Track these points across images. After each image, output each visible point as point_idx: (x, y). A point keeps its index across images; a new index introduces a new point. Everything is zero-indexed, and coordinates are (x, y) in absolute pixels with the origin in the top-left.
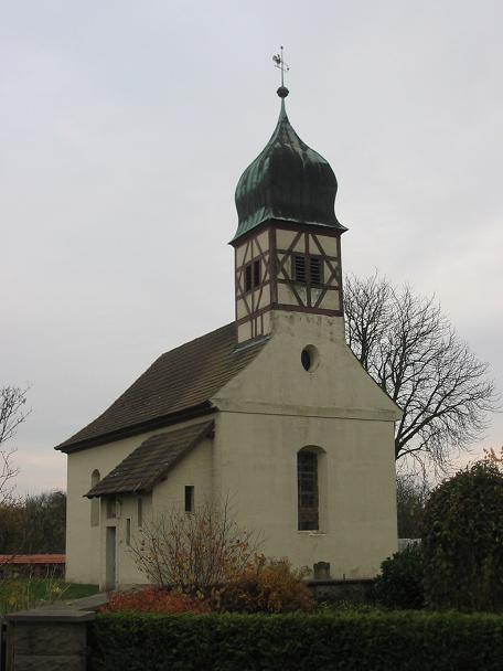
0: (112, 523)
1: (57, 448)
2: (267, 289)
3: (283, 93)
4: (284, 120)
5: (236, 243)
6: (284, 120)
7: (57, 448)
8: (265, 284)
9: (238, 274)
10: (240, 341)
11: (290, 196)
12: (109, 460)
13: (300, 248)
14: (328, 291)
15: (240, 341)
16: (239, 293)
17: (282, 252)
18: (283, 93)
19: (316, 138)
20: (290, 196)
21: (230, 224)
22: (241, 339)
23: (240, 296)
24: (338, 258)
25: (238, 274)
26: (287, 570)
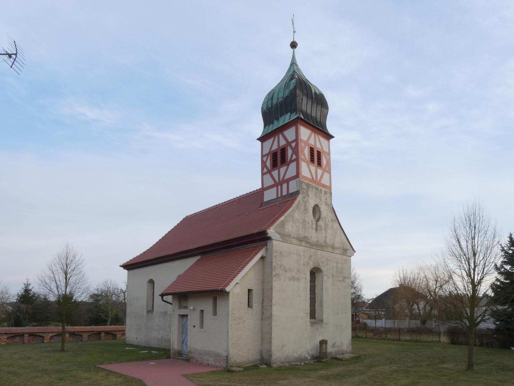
0: (183, 312)
1: (121, 266)
2: (293, 165)
3: (294, 45)
4: (293, 63)
5: (262, 139)
6: (293, 63)
7: (121, 266)
8: (292, 161)
9: (265, 159)
10: (265, 200)
11: (294, 109)
12: (167, 275)
13: (312, 142)
14: (290, 183)
15: (265, 200)
16: (265, 170)
17: (292, 142)
18: (294, 45)
19: (315, 76)
20: (294, 109)
21: (258, 127)
22: (266, 199)
23: (266, 171)
24: (263, 174)
25: (265, 159)
26: (71, 298)
